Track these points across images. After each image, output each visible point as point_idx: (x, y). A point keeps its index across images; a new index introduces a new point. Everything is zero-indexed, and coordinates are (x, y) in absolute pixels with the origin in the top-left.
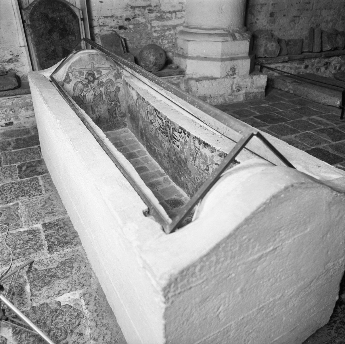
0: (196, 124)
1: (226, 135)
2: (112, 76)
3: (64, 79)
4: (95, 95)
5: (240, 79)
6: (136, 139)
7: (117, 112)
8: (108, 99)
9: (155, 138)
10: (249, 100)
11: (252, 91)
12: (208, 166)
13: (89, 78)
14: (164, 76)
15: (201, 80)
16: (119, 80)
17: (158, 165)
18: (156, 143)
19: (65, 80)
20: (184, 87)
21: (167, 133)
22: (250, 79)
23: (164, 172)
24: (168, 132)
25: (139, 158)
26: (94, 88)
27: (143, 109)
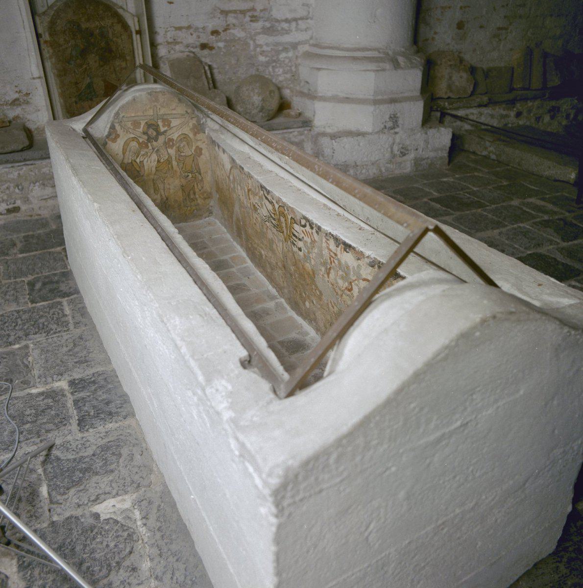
1: (381, 231)
2: (189, 129)
3: (106, 133)
6: (229, 236)
7: (197, 190)
8: (182, 168)
11: (427, 156)
12: (351, 283)
13: (150, 133)
14: (276, 130)
15: (340, 137)
16: (200, 136)
18: (263, 244)
23: (276, 294)
25: (234, 270)
26: (158, 150)
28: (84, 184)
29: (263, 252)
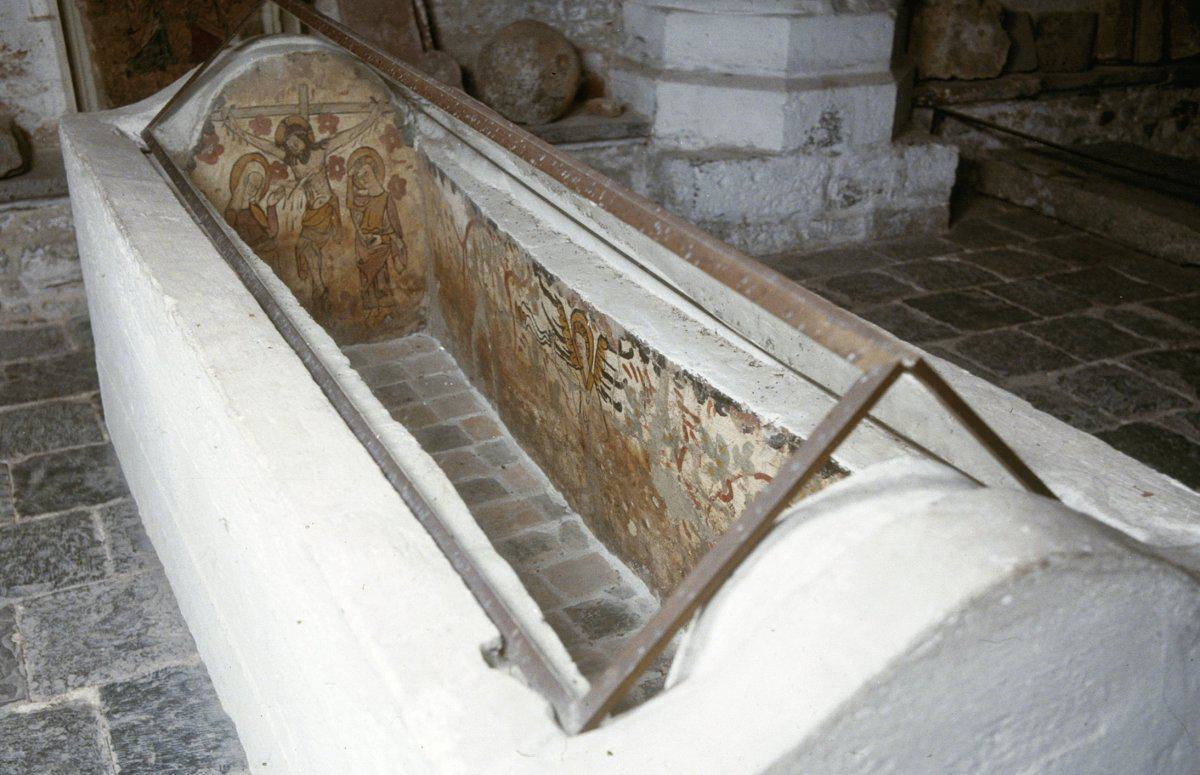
0: (687, 323)
1: (799, 370)
2: (376, 137)
3: (194, 143)
5: (856, 157)
6: (461, 374)
7: (393, 272)
8: (361, 223)
9: (536, 373)
13: (290, 144)
15: (711, 161)
17: (543, 474)
18: (537, 394)
20: (644, 187)
21: (578, 358)
22: (895, 159)
23: (565, 503)
24: (583, 352)
25: (471, 449)
26: (307, 183)
27: (489, 264)
28: (142, 252)
29: (536, 412)
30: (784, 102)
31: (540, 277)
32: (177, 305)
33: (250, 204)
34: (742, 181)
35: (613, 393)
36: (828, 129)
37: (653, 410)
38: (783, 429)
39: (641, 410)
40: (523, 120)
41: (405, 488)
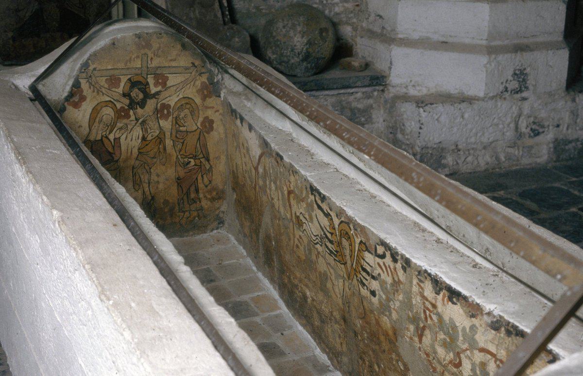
0: (426, 234)
1: (510, 272)
2: (194, 90)
3: (66, 94)
4: (144, 139)
5: (540, 102)
6: (249, 261)
7: (201, 186)
8: (180, 151)
9: (308, 264)
10: (567, 160)
11: (575, 137)
12: (458, 354)
13: (133, 94)
14: (327, 89)
15: (431, 104)
16: (211, 101)
17: (312, 341)
18: (309, 280)
19: (68, 96)
20: (381, 120)
21: (343, 256)
22: (569, 103)
23: (329, 363)
24: (347, 252)
25: (258, 319)
26: (144, 122)
27: (275, 183)
28: (36, 178)
29: (308, 293)
30: (485, 62)
31: (315, 196)
32: (62, 217)
33: (102, 136)
34: (455, 119)
35: (370, 283)
36: (518, 81)
37: (401, 297)
38: (501, 317)
39: (391, 297)
40: (293, 73)
41: (230, 357)
